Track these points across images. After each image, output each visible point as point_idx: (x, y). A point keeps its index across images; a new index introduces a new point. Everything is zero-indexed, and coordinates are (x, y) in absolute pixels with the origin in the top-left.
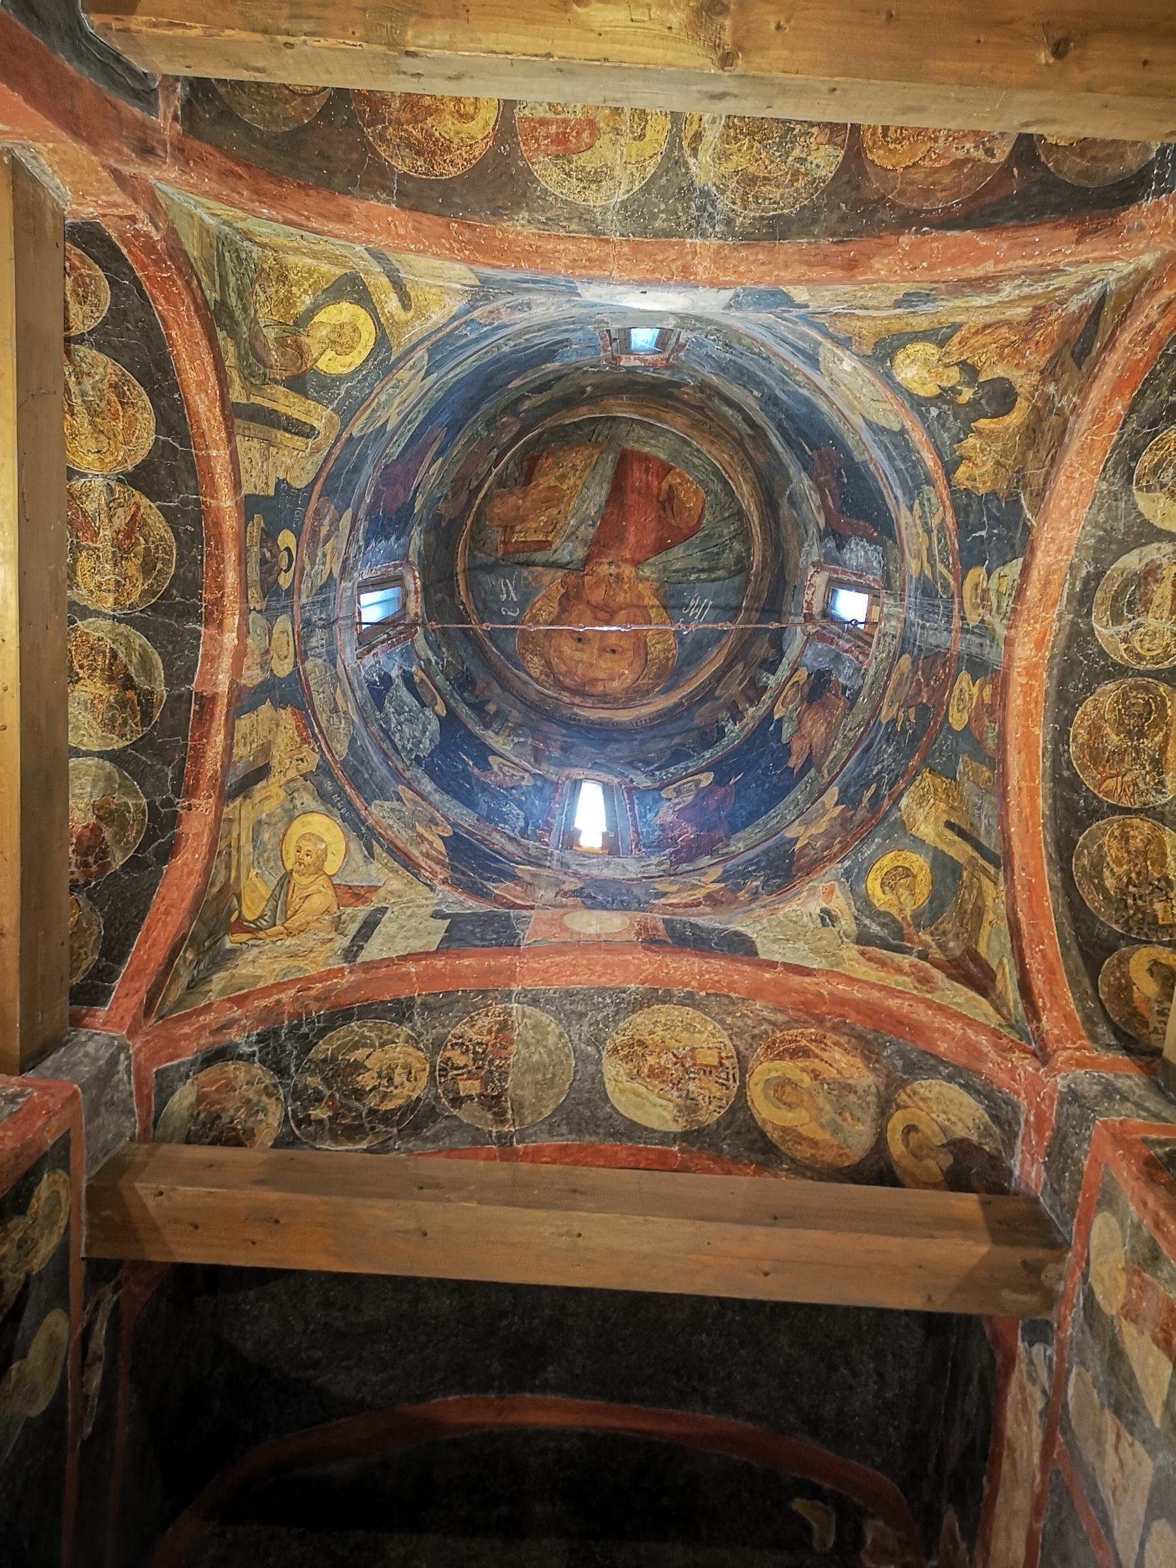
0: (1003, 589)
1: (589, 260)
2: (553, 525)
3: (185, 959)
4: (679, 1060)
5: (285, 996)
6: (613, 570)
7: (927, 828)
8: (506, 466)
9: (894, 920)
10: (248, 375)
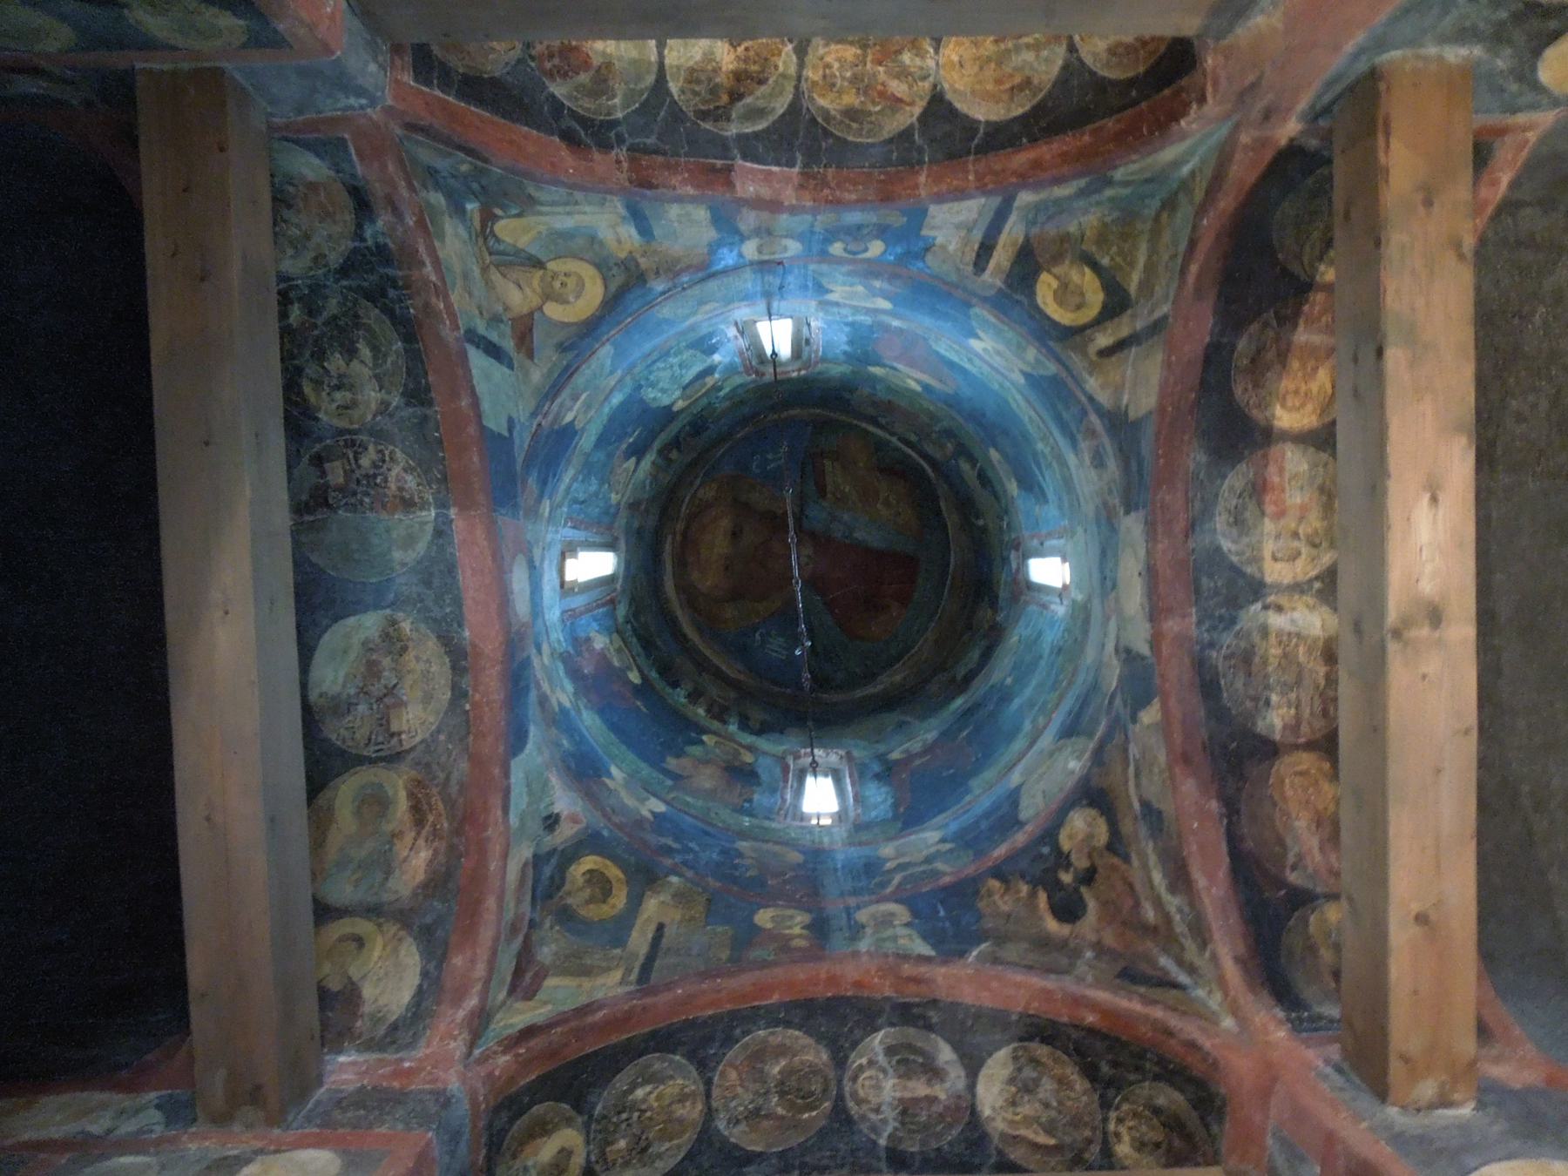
0: (901, 941)
3: (463, 162)
4: (391, 691)
5: (429, 268)
8: (897, 449)
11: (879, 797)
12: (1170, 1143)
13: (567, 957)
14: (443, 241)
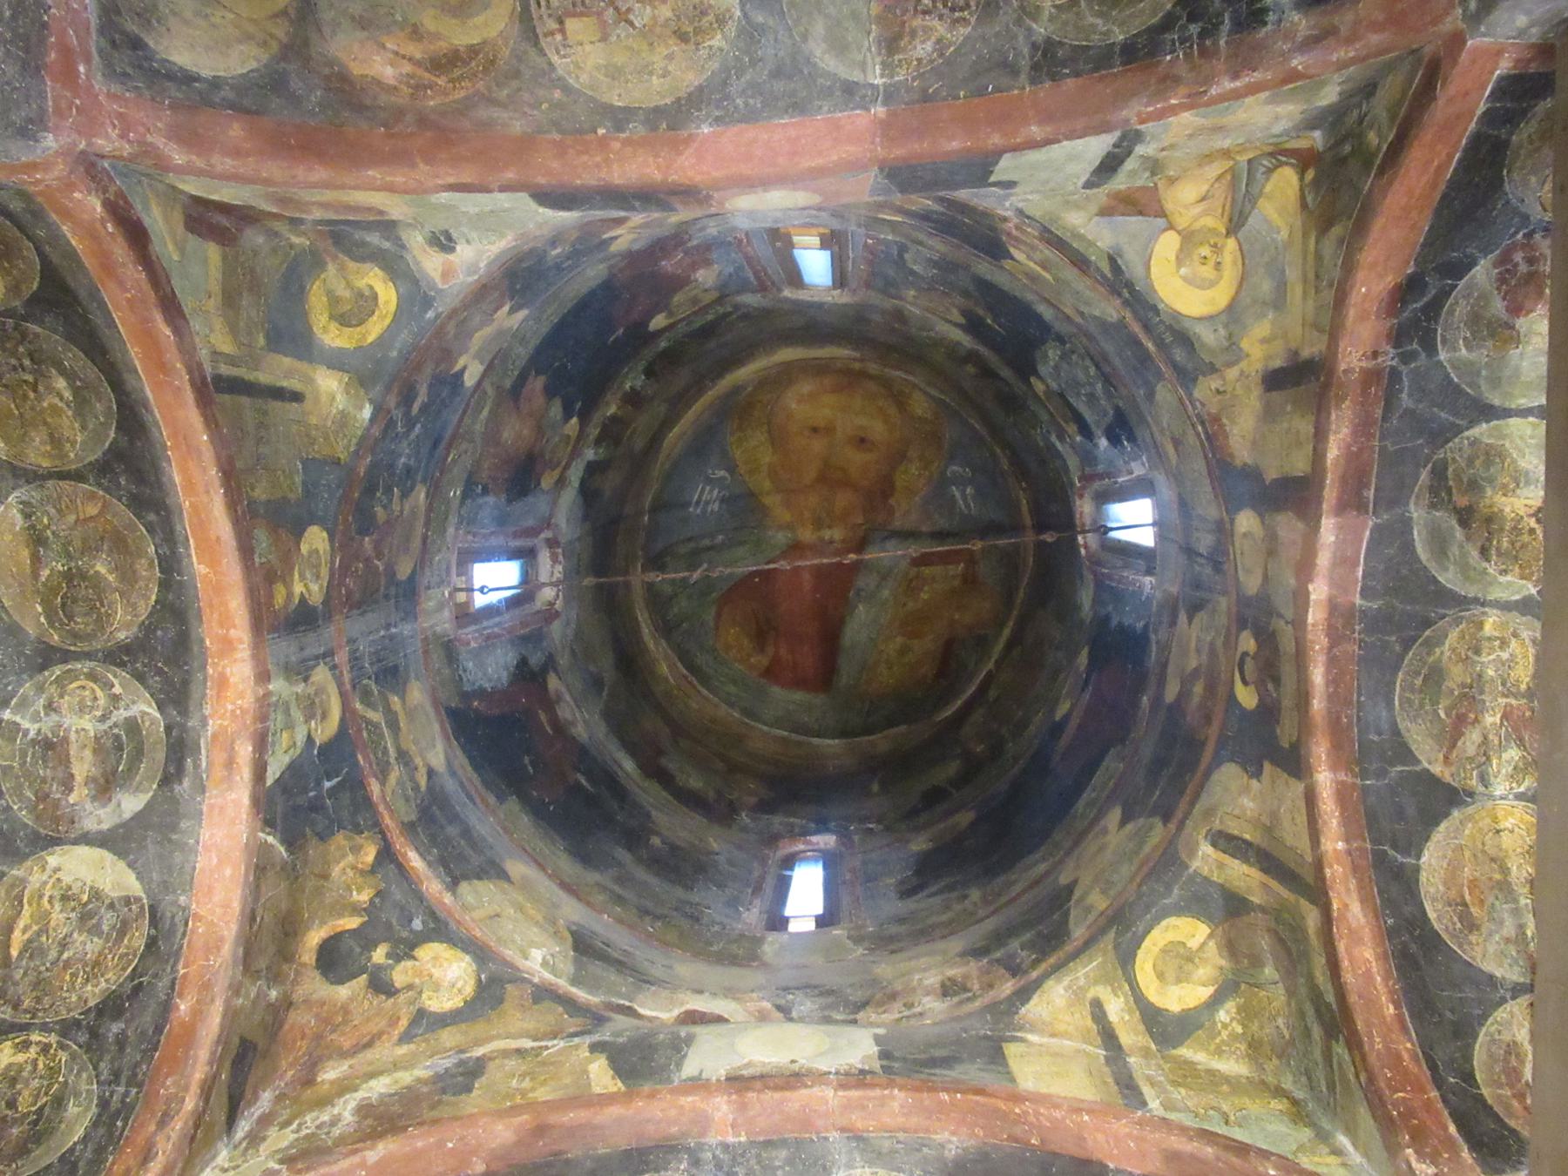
1: (864, 1108)
5: (1228, 85)
6: (827, 534)
7: (329, 385)
10: (1298, 930)
11: (492, 668)
12: (15, 1121)
13: (252, 271)
14: (1269, 102)
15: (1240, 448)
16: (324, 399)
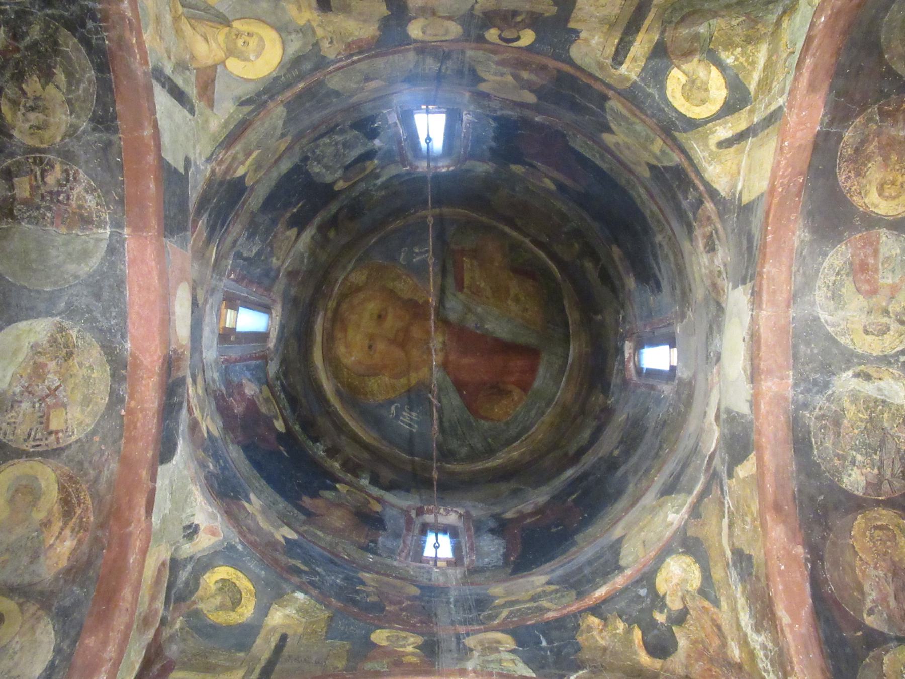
1: (774, 292)
2: (476, 292)
9: (192, 593)
11: (492, 548)
15: (367, 31)
16: (287, 622)
